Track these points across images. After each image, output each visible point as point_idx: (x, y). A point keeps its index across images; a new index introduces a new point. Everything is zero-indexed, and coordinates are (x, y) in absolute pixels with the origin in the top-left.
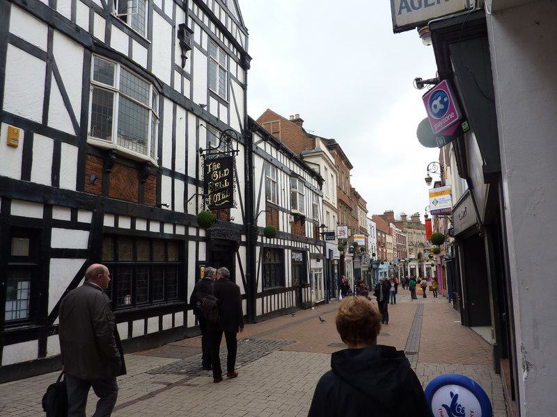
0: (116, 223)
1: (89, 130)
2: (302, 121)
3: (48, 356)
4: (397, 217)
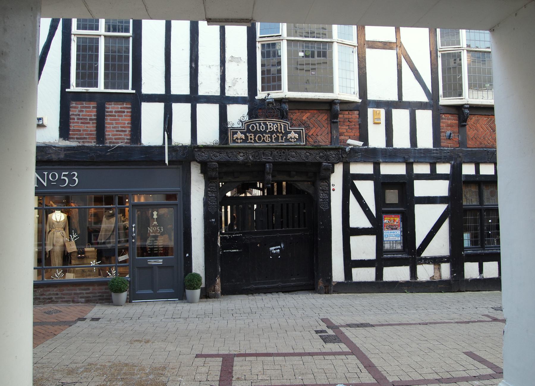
0: (477, 170)
1: (441, 92)
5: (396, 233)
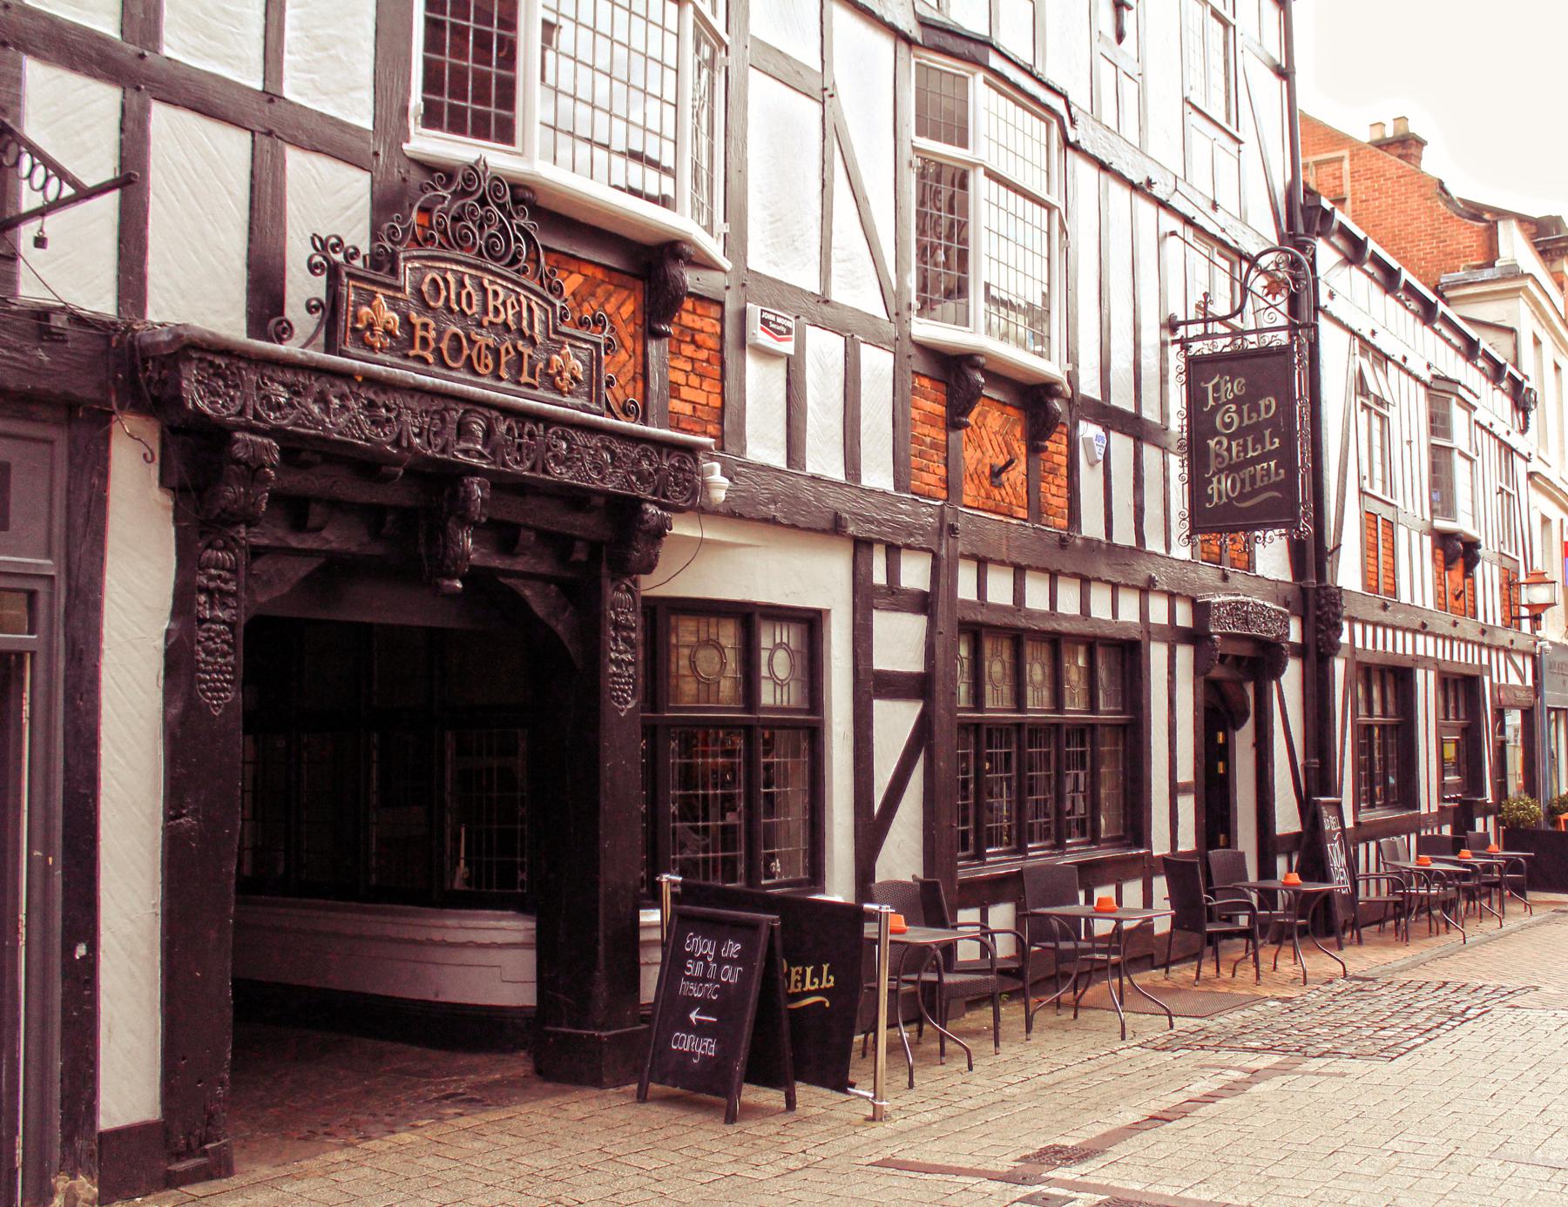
2: (1421, 143)
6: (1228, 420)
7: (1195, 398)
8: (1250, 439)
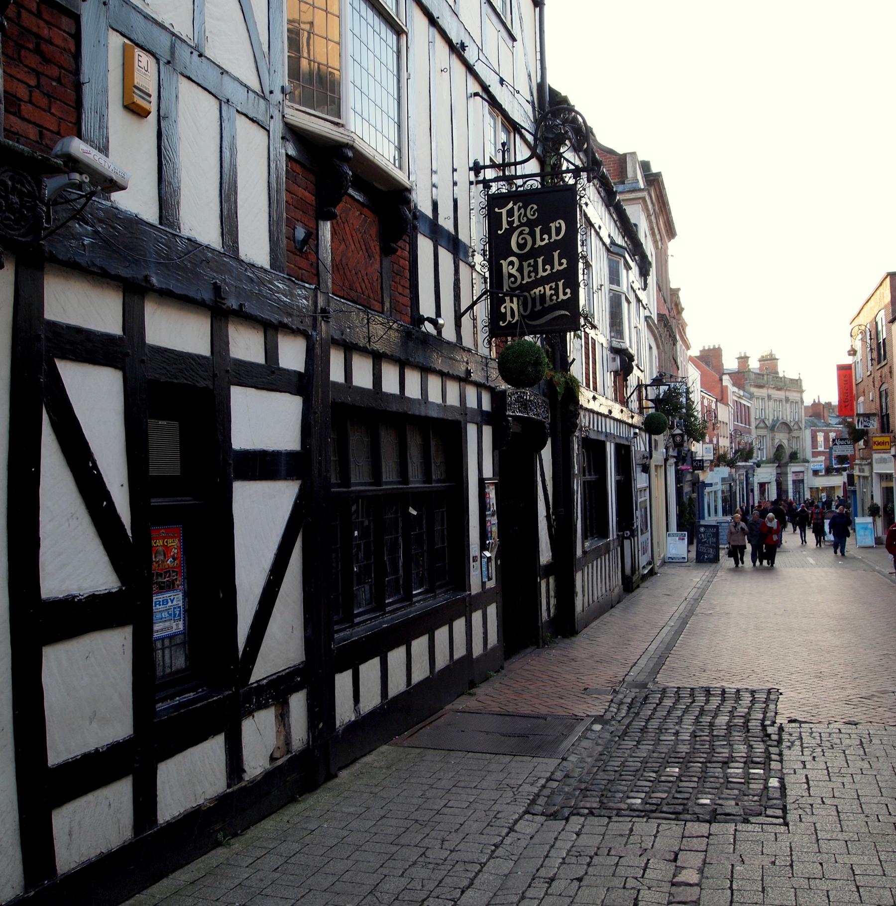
3: (247, 777)
4: (730, 363)
5: (172, 602)
6: (521, 242)
7: (493, 220)
8: (540, 260)
